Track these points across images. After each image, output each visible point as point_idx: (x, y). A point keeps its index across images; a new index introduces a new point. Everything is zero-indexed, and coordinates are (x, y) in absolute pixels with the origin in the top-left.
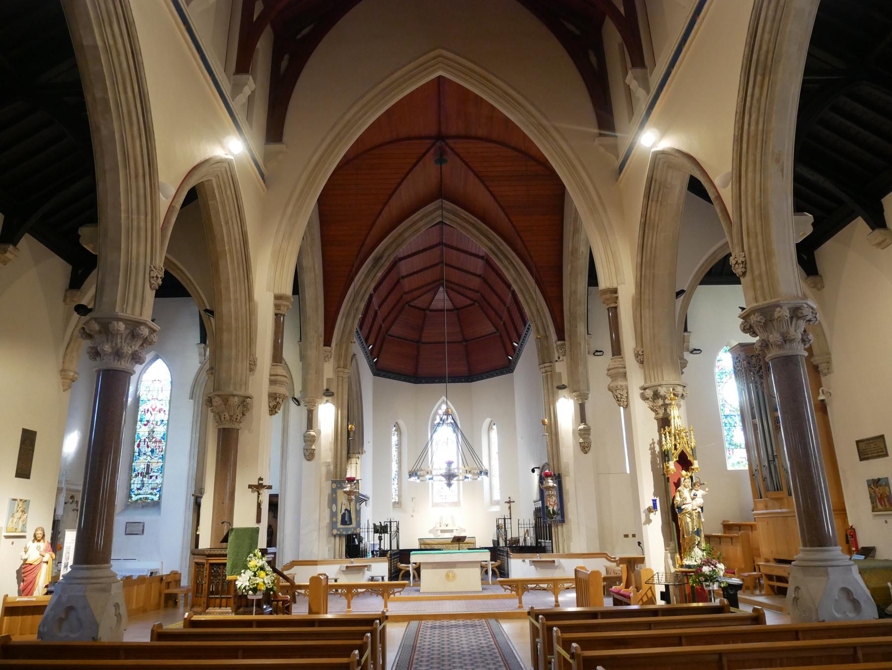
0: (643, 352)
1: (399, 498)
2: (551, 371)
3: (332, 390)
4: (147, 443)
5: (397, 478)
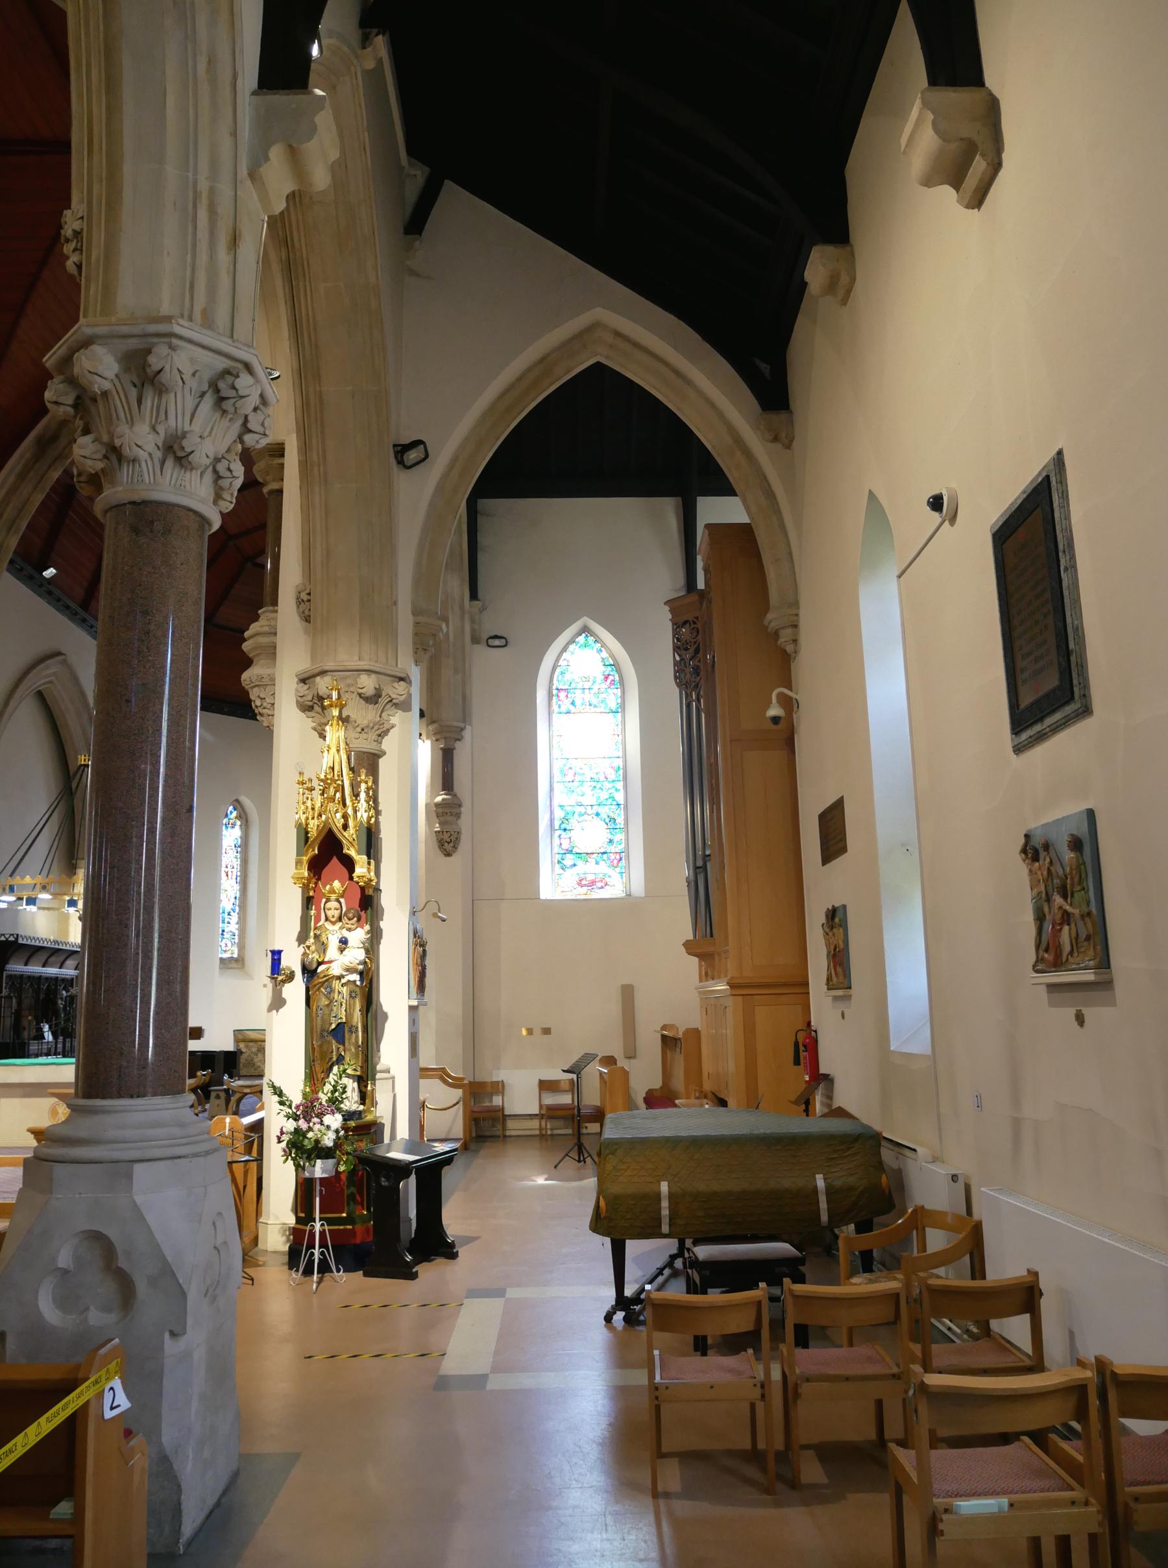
0: (309, 594)
1: (239, 951)
5: (237, 910)
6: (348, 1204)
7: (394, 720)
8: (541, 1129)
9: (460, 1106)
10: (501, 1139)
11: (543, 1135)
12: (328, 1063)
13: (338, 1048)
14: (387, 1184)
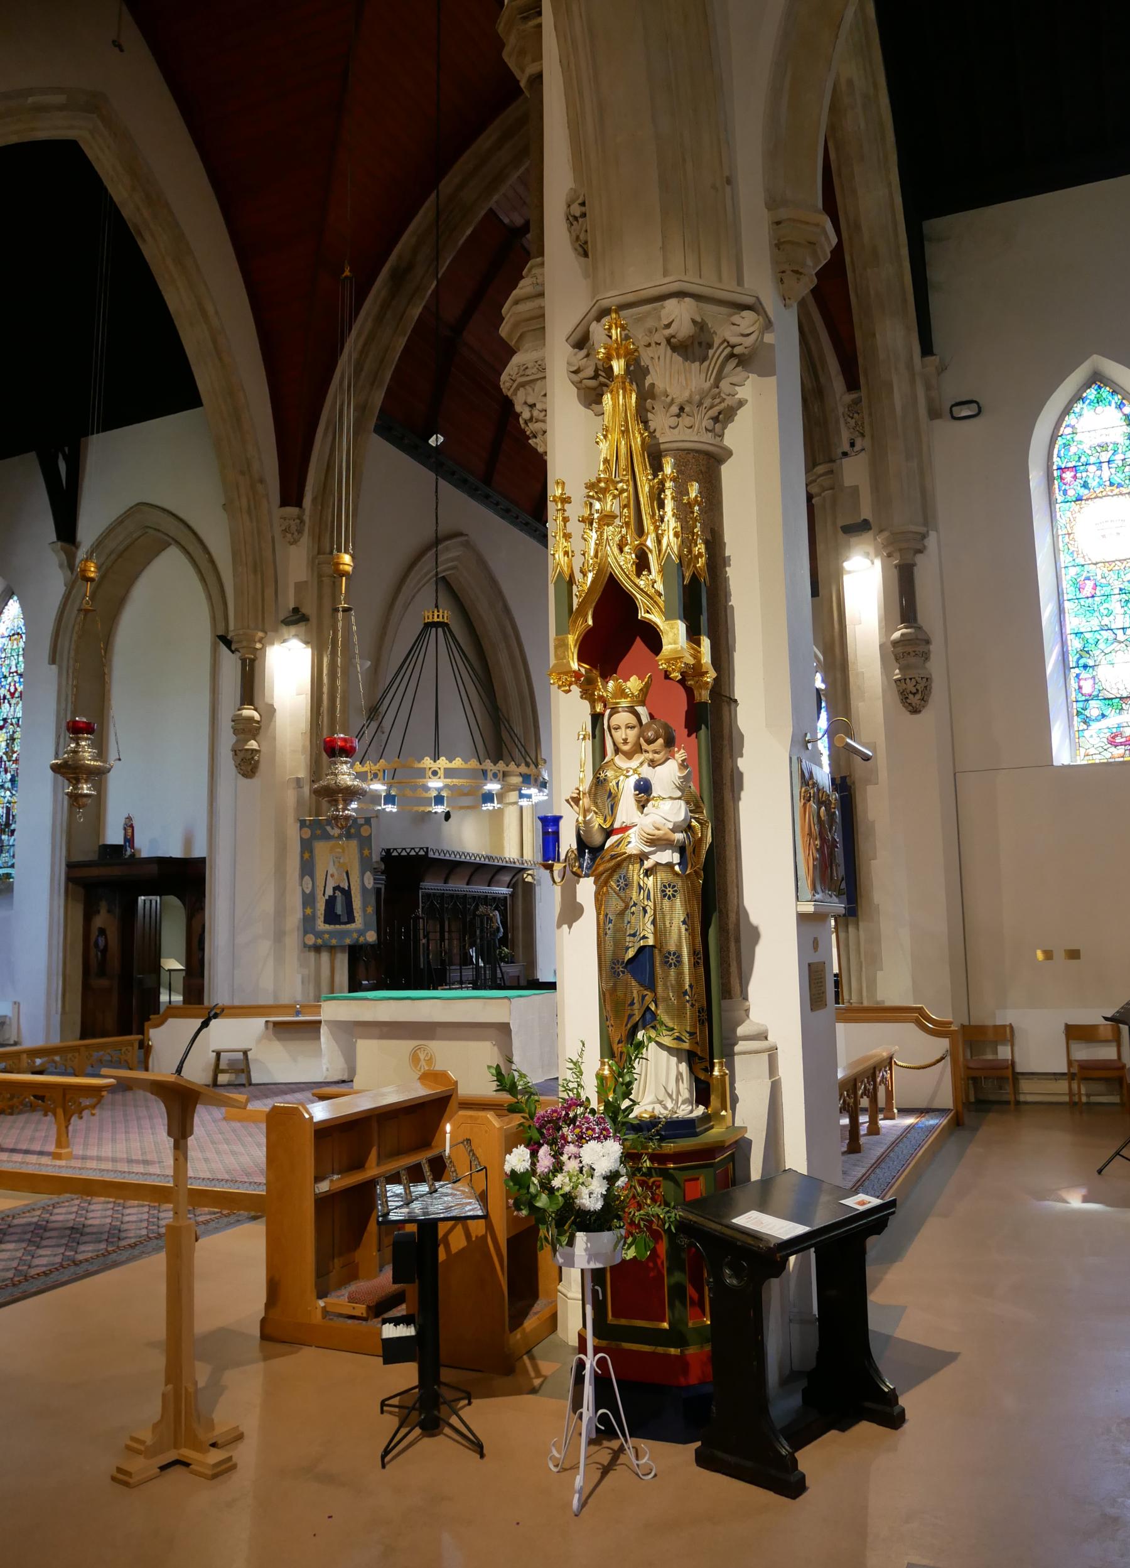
2: (832, 488)
3: (304, 610)
4: (5, 765)
6: (672, 1306)
7: (742, 393)
8: (1071, 1094)
9: (947, 1062)
10: (1012, 1106)
11: (1075, 1104)
12: (626, 1025)
13: (644, 997)
14: (735, 1282)
